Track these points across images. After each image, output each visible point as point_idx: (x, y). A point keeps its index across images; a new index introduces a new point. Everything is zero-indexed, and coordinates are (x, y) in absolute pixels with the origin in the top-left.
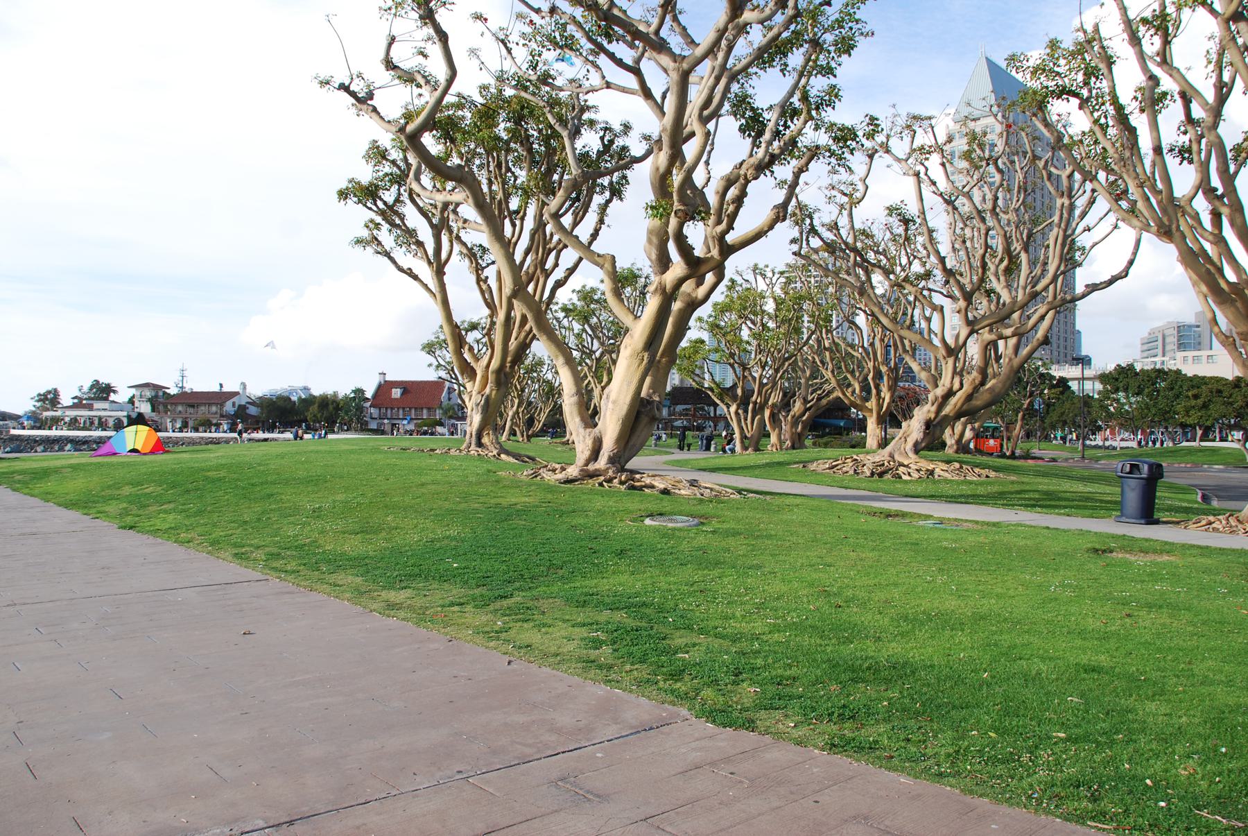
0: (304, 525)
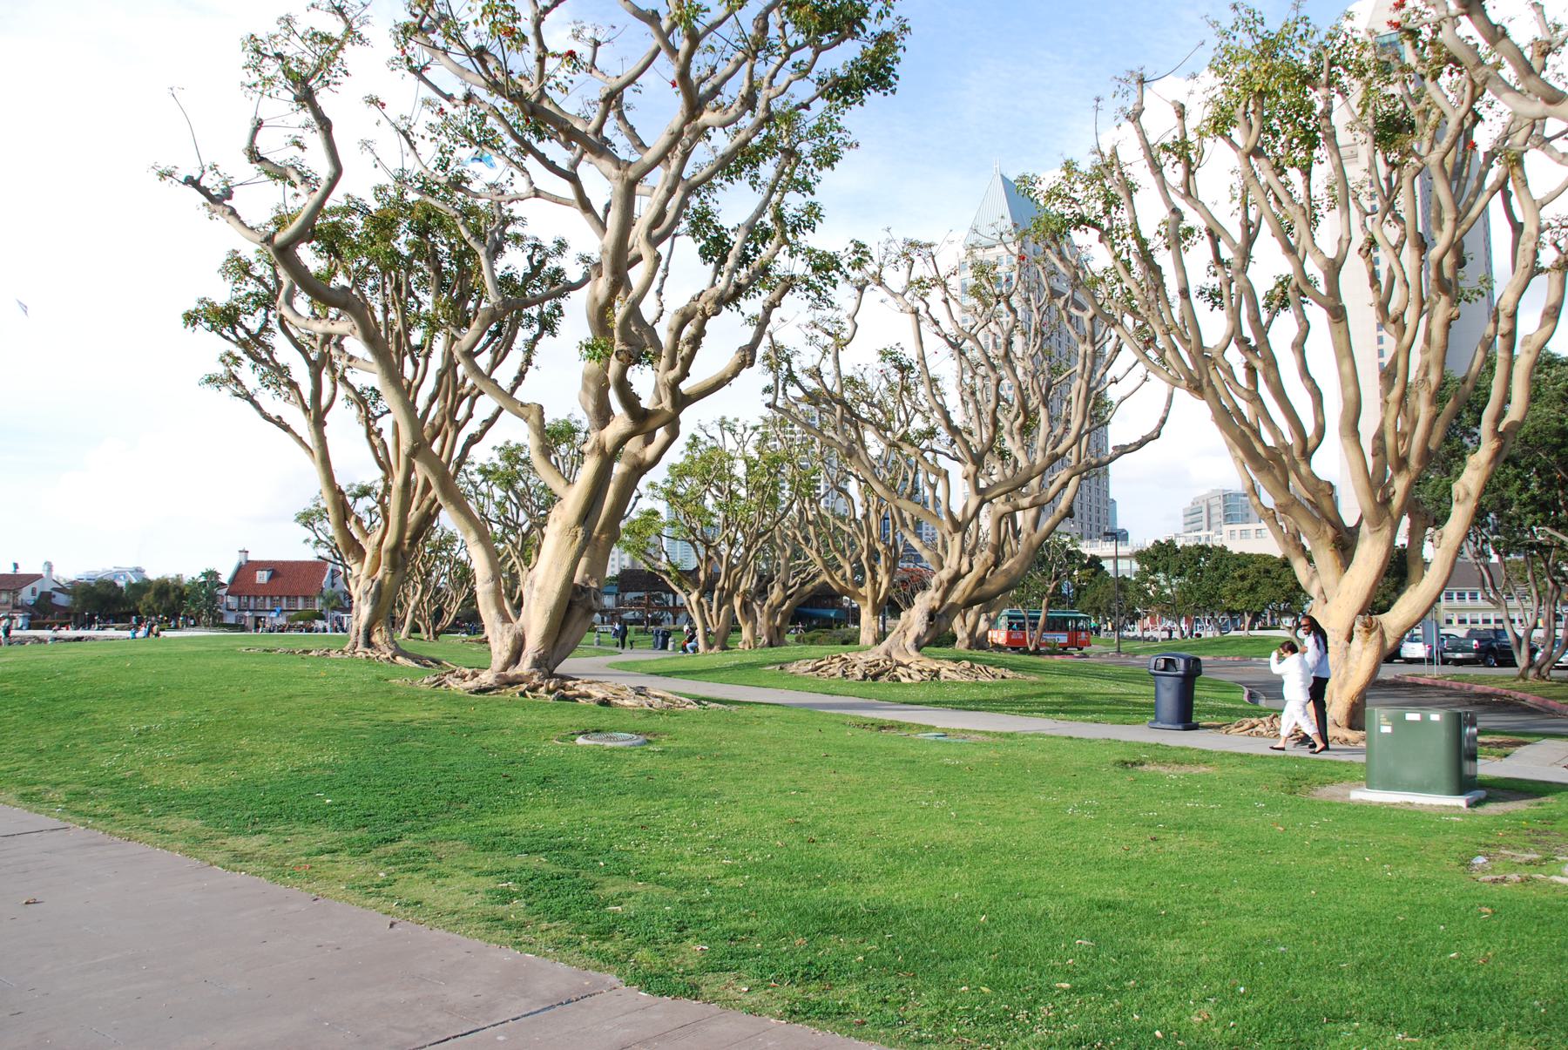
0: (126, 750)
